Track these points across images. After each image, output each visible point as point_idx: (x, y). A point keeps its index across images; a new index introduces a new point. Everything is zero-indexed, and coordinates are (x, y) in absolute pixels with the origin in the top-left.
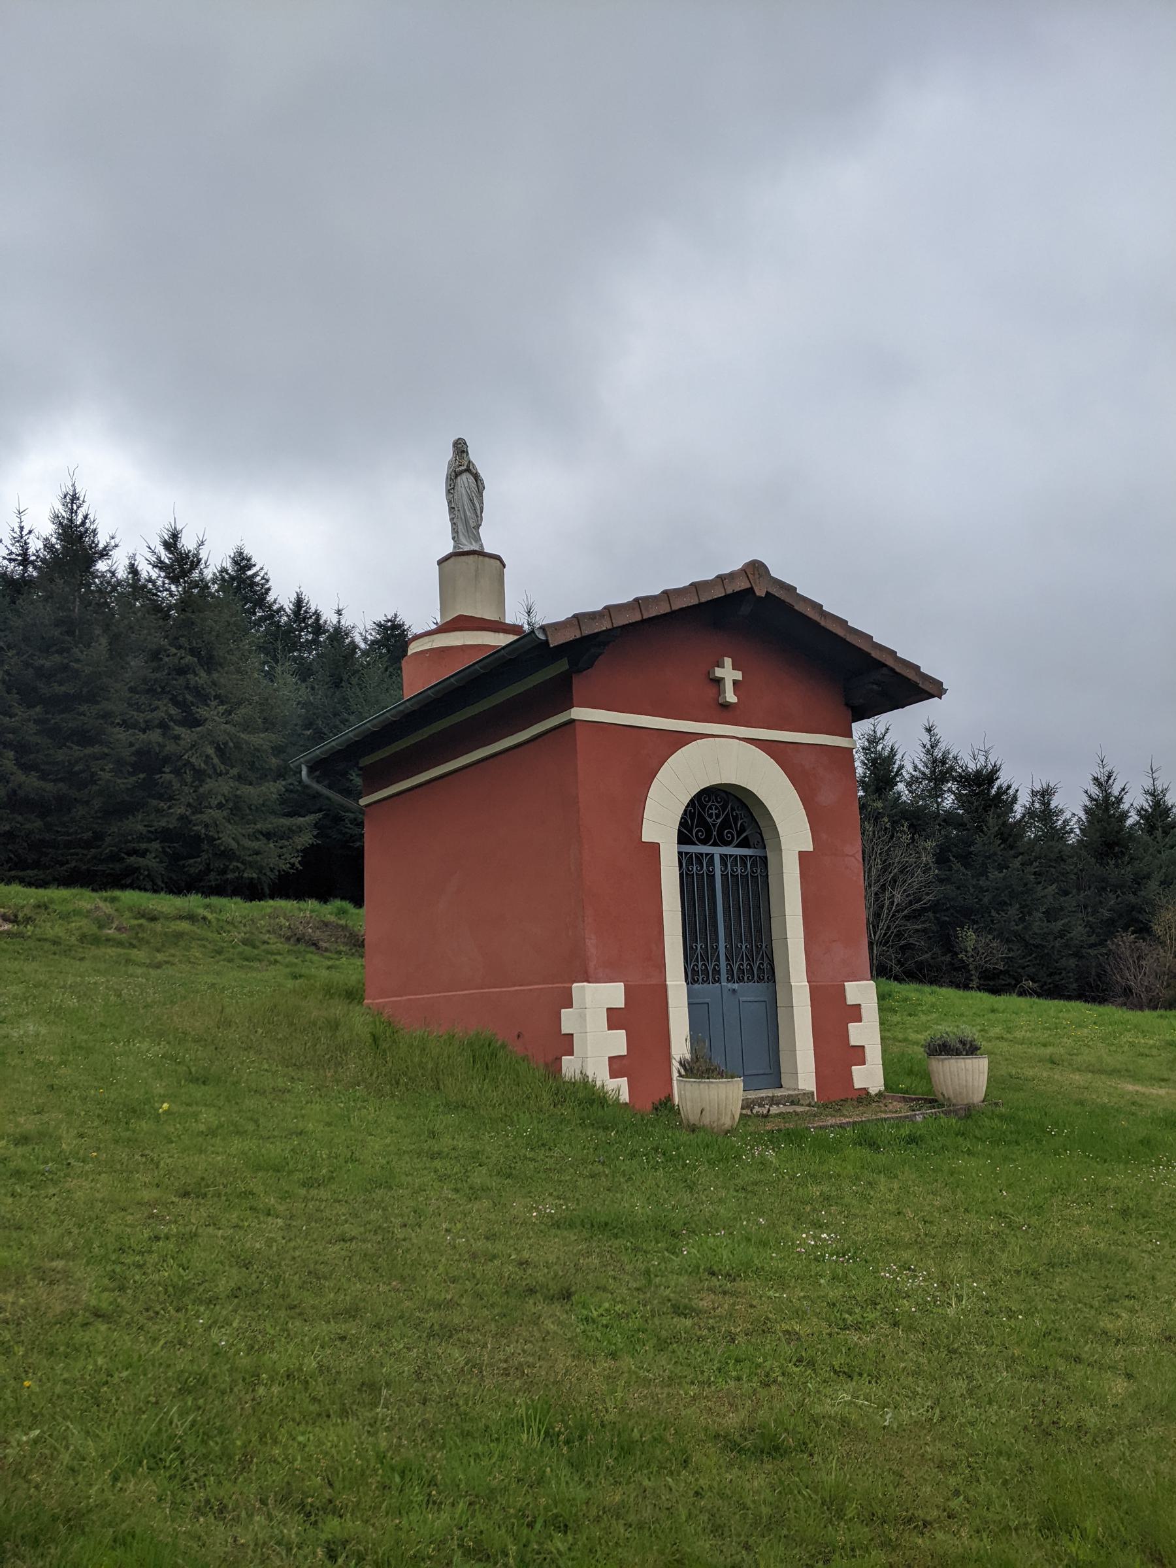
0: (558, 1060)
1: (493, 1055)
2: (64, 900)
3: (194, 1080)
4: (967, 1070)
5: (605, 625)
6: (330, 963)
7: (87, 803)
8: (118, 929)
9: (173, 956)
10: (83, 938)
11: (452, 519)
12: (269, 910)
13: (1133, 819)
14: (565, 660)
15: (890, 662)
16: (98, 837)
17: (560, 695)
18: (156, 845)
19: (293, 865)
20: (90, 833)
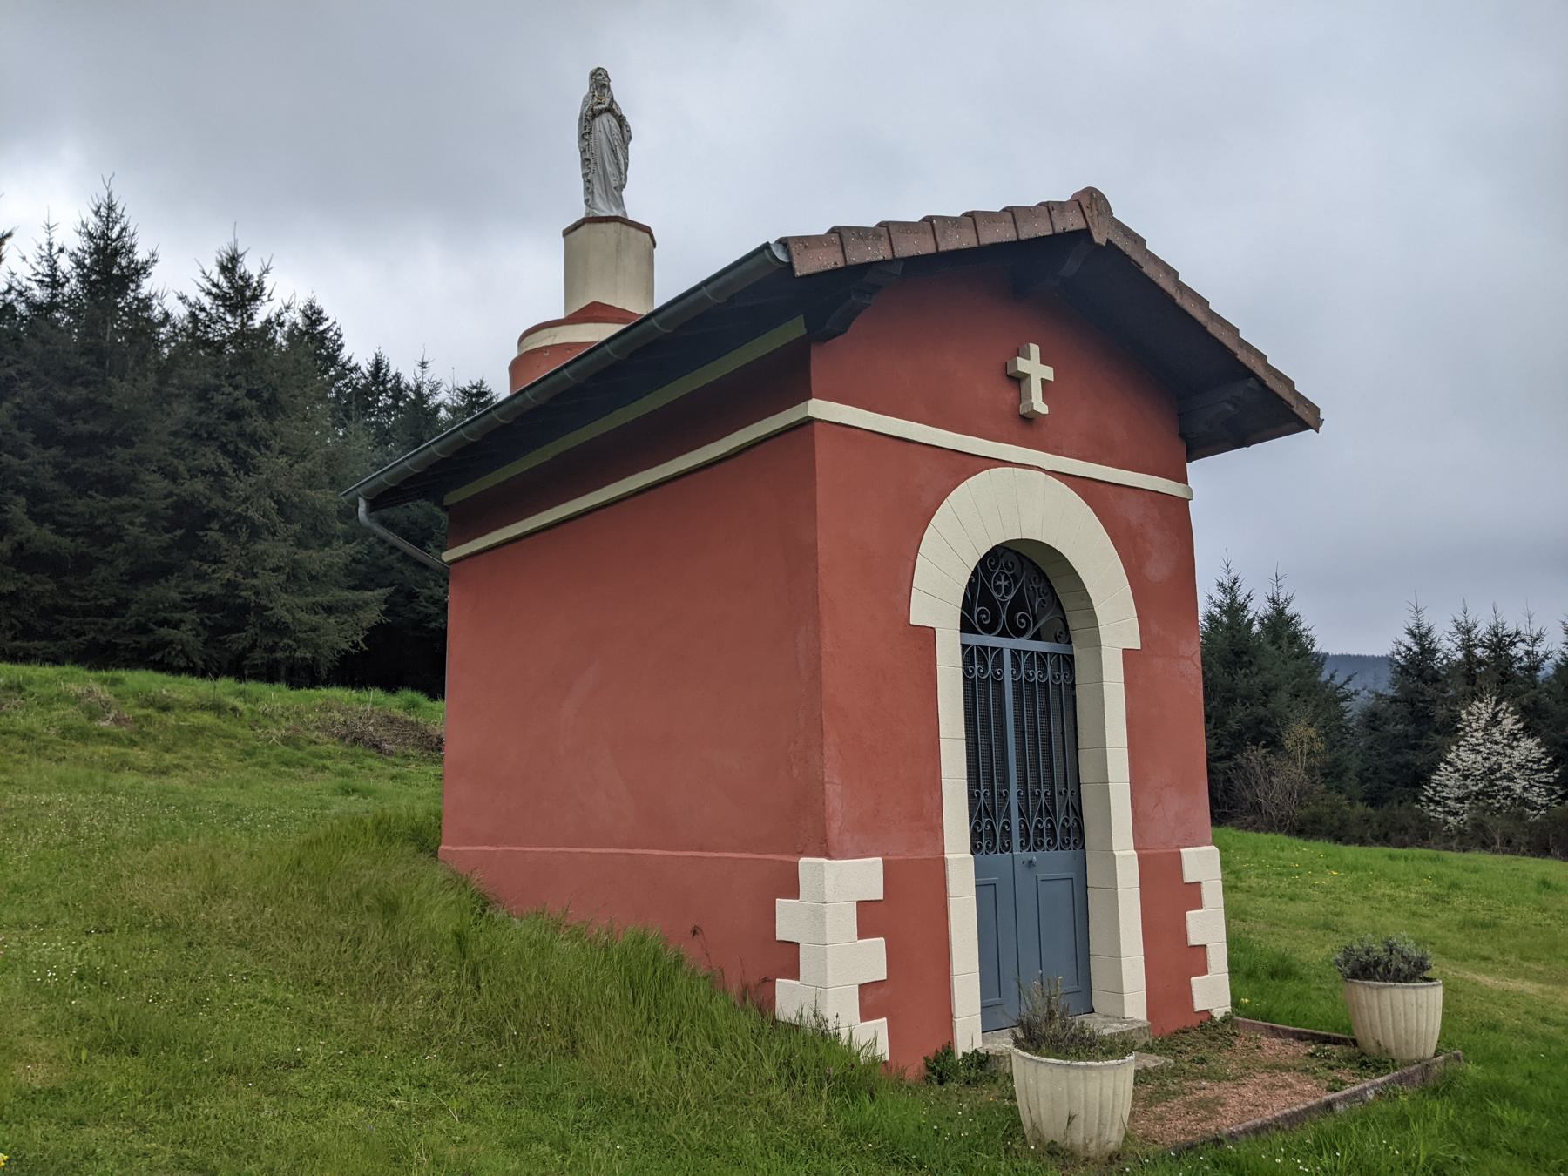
0: (769, 983)
1: (667, 980)
2: (49, 681)
3: (111, 1046)
4: (1419, 1007)
5: (880, 252)
6: (395, 771)
7: (111, 563)
8: (117, 721)
9: (188, 758)
10: (66, 732)
11: (585, 175)
12: (320, 701)
13: (1256, 628)
14: (800, 320)
15: (1260, 371)
16: (123, 604)
17: (788, 379)
18: (192, 616)
19: (356, 645)
20: (113, 600)
